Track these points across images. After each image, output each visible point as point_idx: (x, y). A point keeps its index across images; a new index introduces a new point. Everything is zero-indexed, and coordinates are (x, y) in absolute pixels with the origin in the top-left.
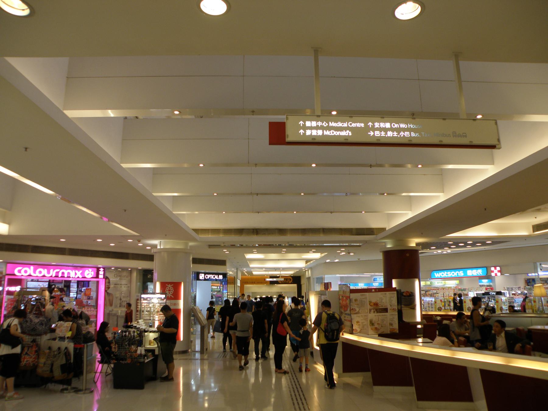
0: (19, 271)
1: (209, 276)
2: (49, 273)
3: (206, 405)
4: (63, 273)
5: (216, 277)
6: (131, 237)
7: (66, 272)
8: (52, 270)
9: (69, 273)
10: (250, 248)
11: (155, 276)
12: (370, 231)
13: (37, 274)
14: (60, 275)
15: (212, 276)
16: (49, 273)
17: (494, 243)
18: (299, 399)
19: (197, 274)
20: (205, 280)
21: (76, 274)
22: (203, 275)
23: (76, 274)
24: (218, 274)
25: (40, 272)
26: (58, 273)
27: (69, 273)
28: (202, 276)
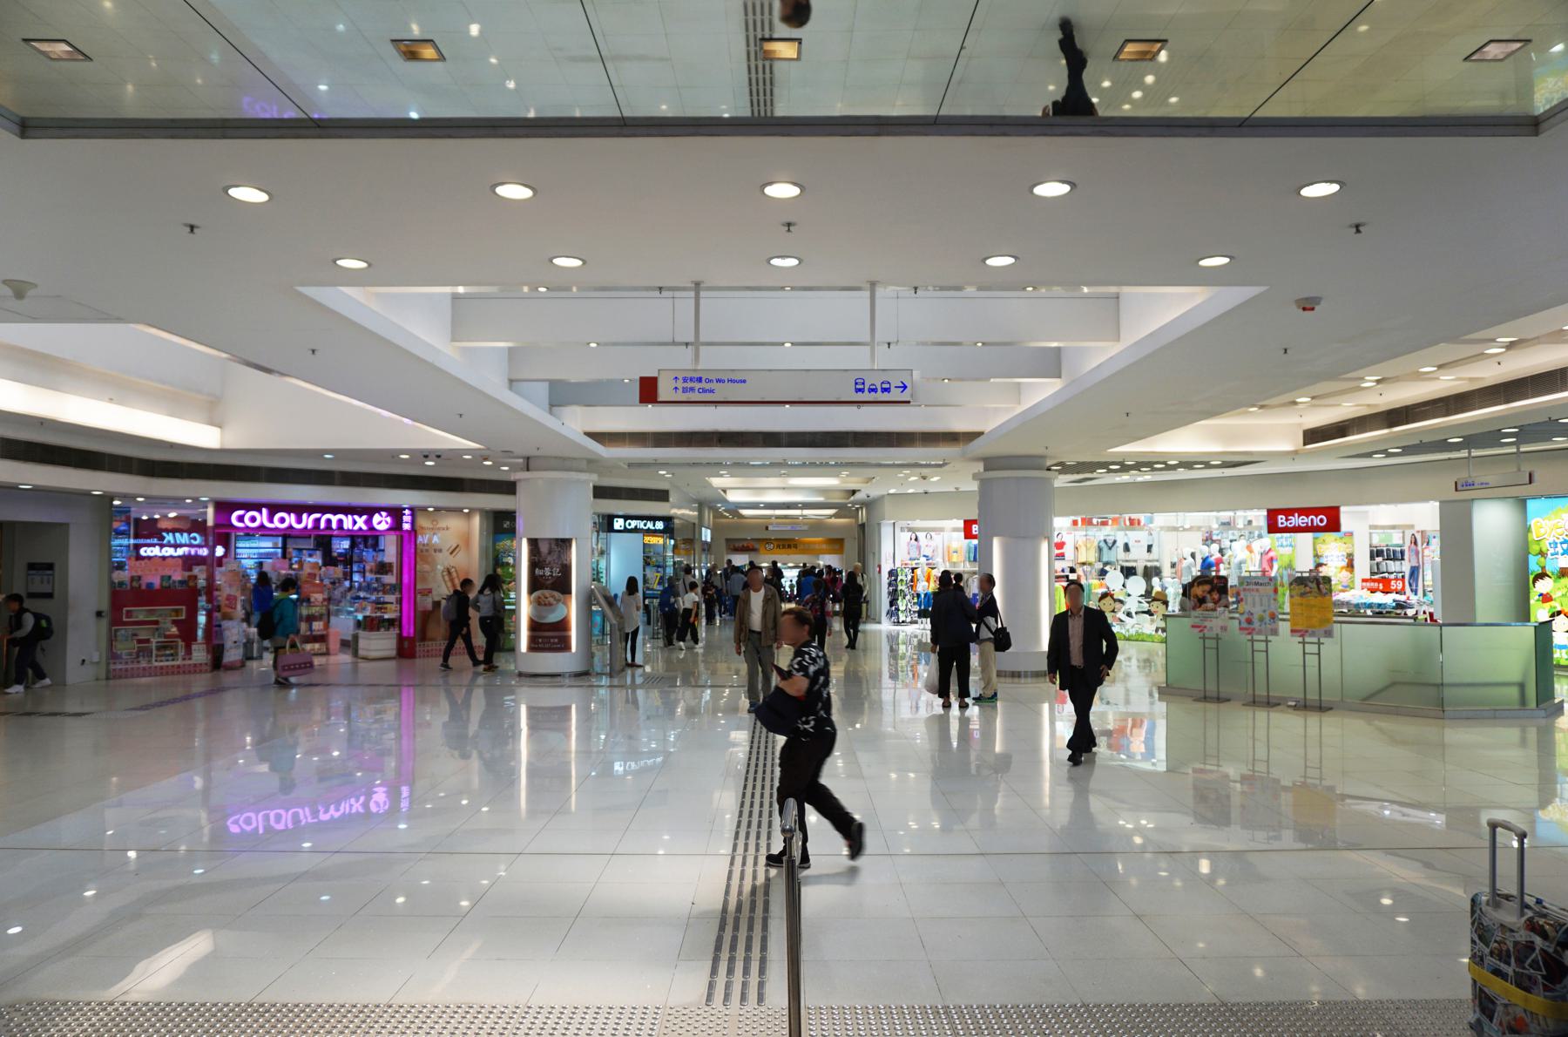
0: (241, 519)
1: (634, 523)
2: (299, 521)
3: (248, 739)
4: (329, 521)
5: (650, 525)
6: (468, 451)
7: (334, 519)
8: (305, 516)
9: (340, 522)
10: (716, 466)
11: (520, 524)
12: (952, 438)
13: (277, 524)
14: (323, 525)
15: (641, 524)
16: (299, 521)
17: (1226, 465)
18: (758, 796)
19: (610, 519)
20: (626, 530)
21: (355, 522)
22: (621, 521)
23: (355, 522)
24: (654, 519)
25: (282, 520)
26: (317, 521)
27: (340, 522)
28: (619, 524)
